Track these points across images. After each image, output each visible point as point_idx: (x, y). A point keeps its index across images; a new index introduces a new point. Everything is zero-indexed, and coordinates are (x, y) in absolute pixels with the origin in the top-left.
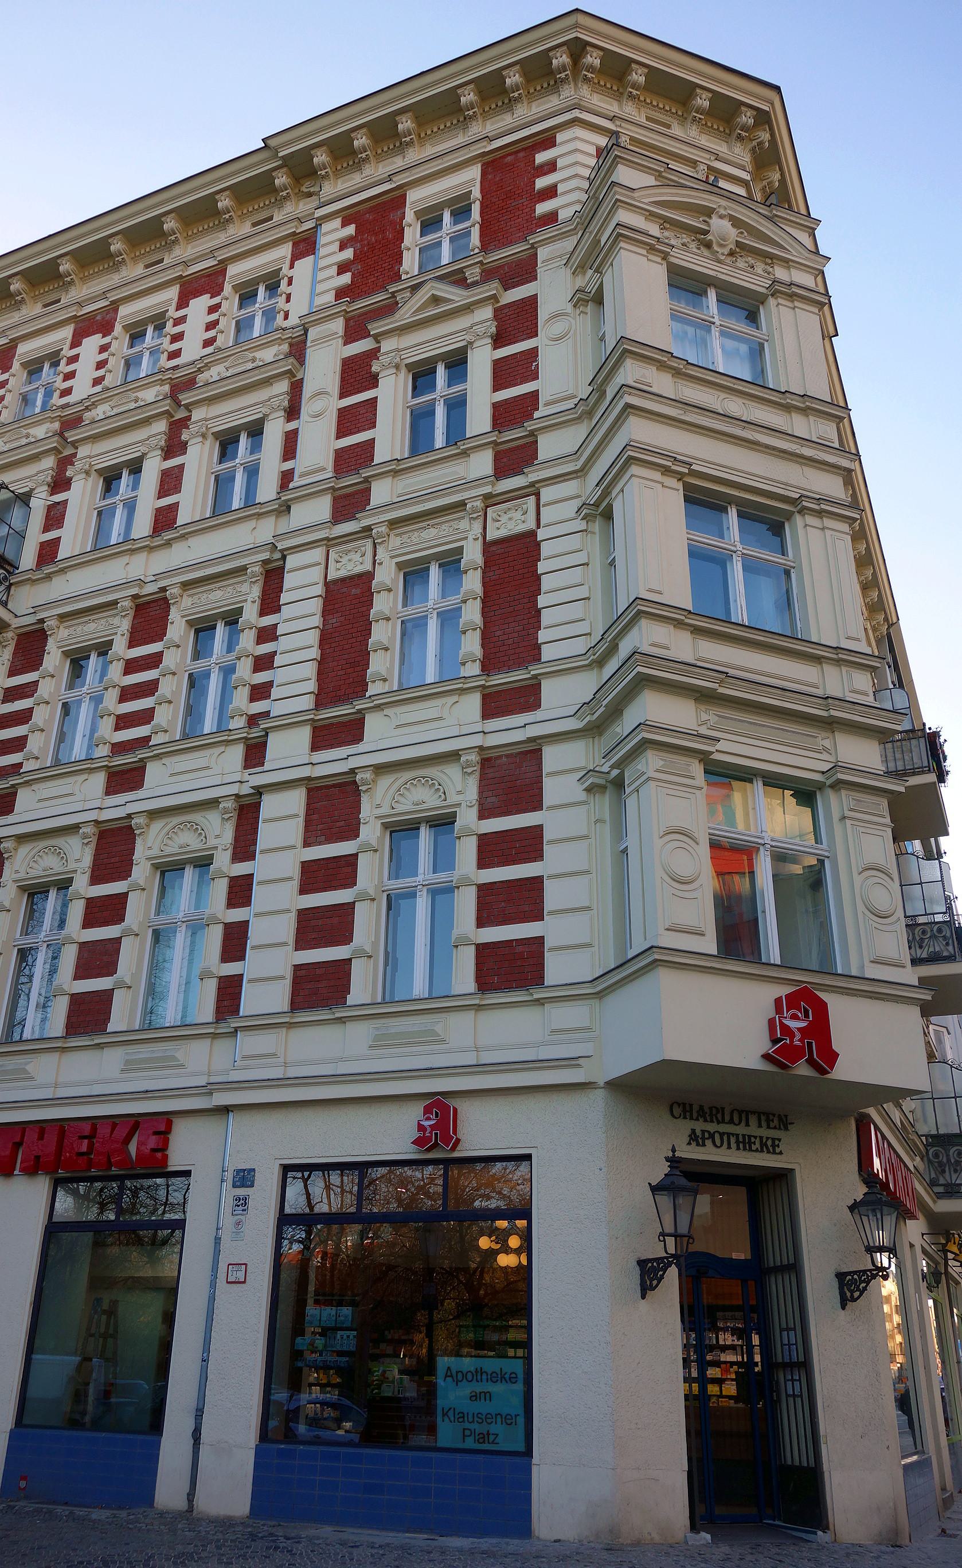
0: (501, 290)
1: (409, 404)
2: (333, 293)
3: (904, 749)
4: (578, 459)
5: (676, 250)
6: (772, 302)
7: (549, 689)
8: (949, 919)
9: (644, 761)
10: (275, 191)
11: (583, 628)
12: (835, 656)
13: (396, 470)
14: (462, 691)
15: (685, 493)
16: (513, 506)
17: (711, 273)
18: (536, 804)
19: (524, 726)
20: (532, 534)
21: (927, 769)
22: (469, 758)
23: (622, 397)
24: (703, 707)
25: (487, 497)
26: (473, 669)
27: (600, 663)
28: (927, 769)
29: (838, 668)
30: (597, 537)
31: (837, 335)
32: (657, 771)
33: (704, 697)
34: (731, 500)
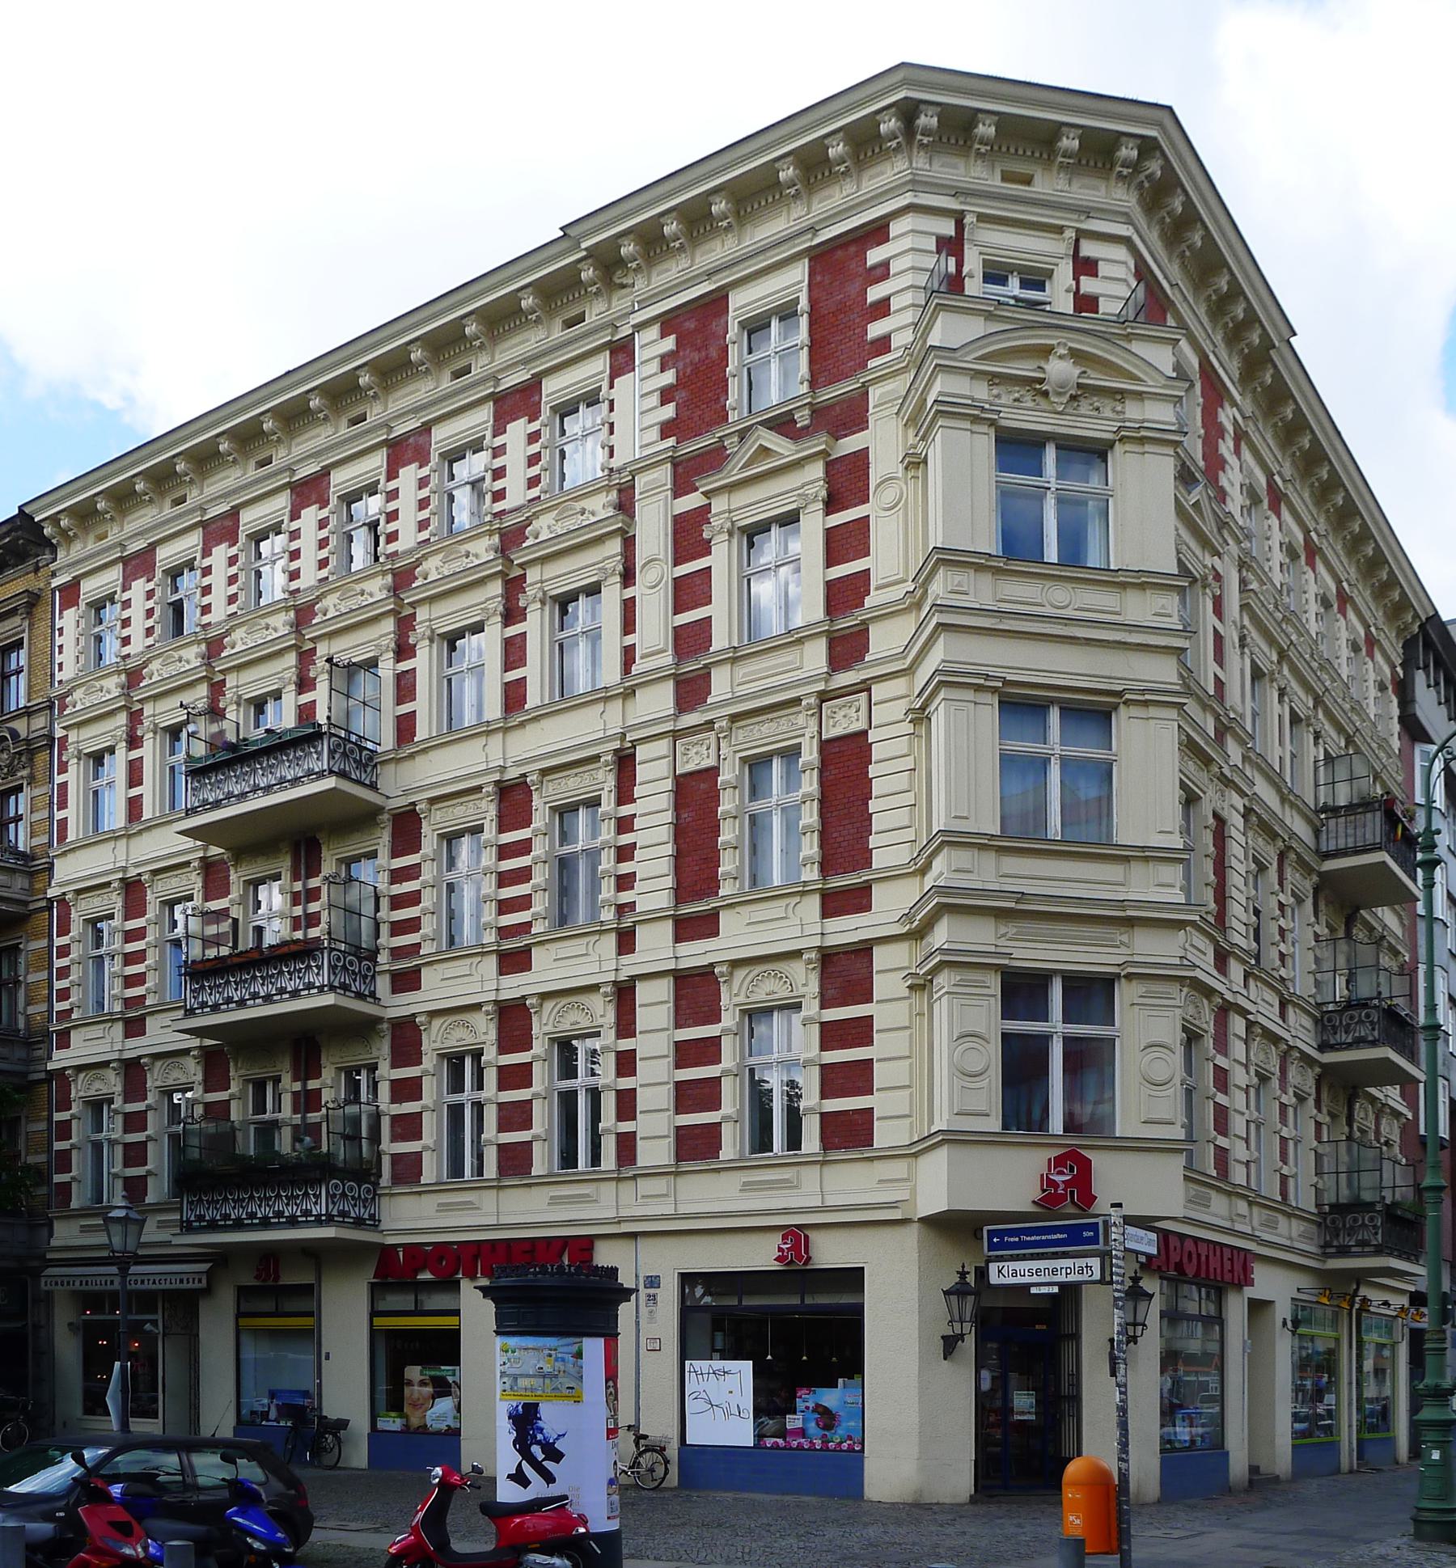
0: (831, 441)
2: (657, 428)
4: (905, 658)
11: (909, 834)
13: (735, 658)
18: (867, 998)
26: (811, 874)
31: (1295, 334)
33: (1001, 914)
34: (1052, 701)
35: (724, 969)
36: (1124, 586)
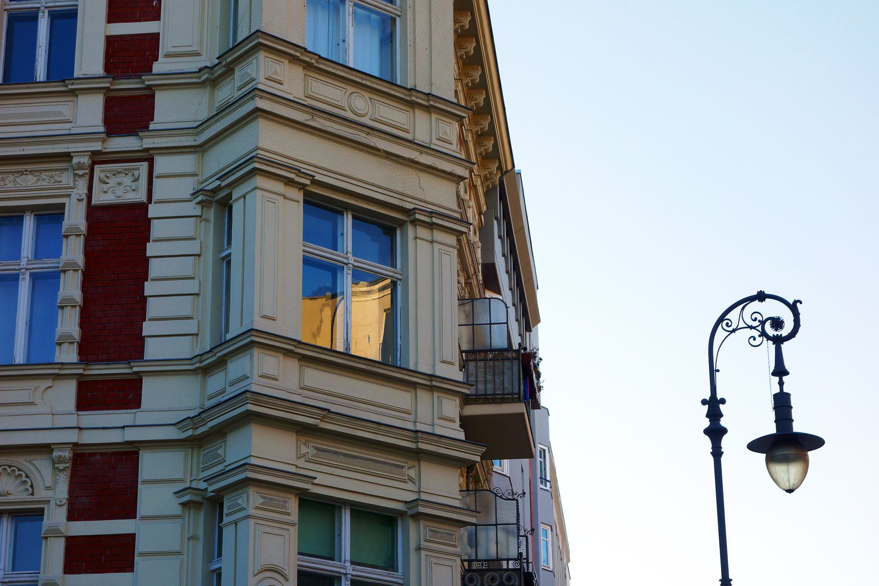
1: (7, 7)
3: (497, 370)
4: (197, 134)
7: (149, 387)
8: (519, 567)
9: (245, 495)
12: (428, 383)
14: (57, 377)
15: (305, 198)
16: (123, 169)
18: (129, 510)
19: (124, 427)
20: (142, 208)
21: (517, 396)
22: (61, 453)
23: (252, 98)
24: (303, 439)
25: (94, 153)
26: (69, 354)
27: (206, 371)
28: (517, 396)
29: (430, 394)
30: (211, 226)
32: (257, 508)
34: (347, 207)
36: (413, 105)
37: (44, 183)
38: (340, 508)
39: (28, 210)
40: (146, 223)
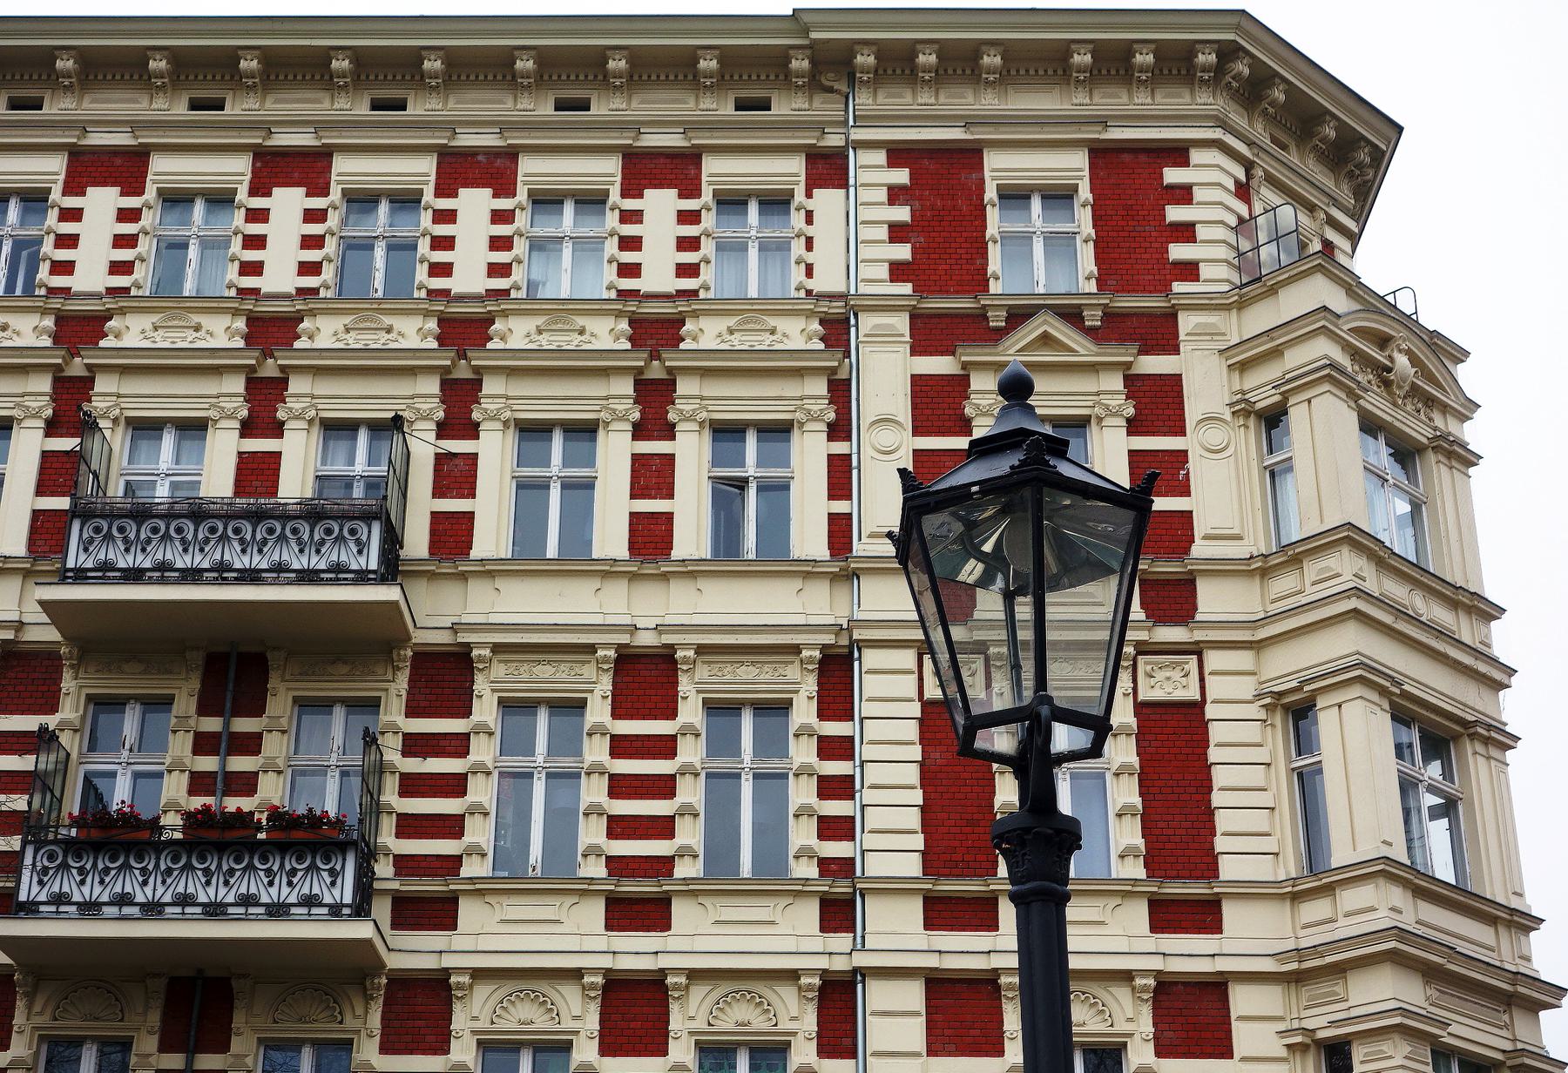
5: (1372, 394)
6: (1431, 457)
10: (788, 74)
14: (797, 894)
17: (1389, 419)
20: (1198, 707)
35: (465, 979)
37: (767, 676)
38: (735, 1050)
39: (339, 701)
40: (1203, 725)
